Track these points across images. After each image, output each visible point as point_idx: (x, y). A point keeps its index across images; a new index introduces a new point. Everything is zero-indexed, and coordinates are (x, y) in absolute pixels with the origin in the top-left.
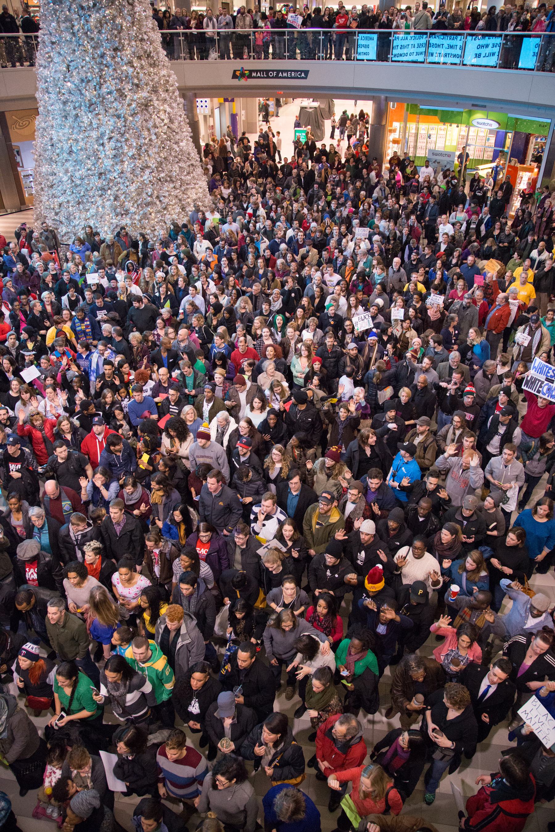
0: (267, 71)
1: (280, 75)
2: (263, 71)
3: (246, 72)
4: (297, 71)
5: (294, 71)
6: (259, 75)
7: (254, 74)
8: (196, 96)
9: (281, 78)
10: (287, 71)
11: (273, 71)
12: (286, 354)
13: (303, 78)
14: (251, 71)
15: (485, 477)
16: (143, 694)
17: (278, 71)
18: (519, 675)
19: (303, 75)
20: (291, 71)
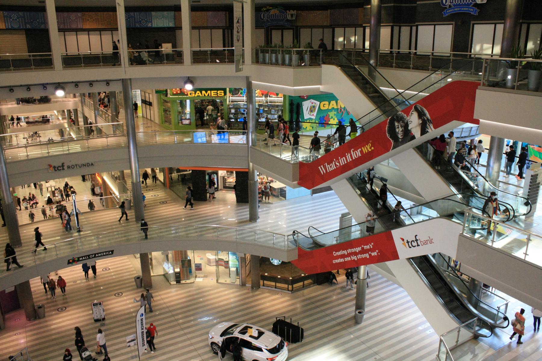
0: (89, 256)
1: (97, 255)
2: (86, 256)
3: (76, 259)
4: (107, 252)
5: (105, 252)
6: (84, 258)
7: (81, 259)
8: (272, 29)
9: (97, 257)
10: (101, 253)
11: (92, 255)
12: (291, 122)
13: (111, 254)
14: (79, 258)
15: (322, 40)
16: (506, 153)
17: (95, 254)
18: (379, 195)
19: (110, 253)
20: (103, 252)
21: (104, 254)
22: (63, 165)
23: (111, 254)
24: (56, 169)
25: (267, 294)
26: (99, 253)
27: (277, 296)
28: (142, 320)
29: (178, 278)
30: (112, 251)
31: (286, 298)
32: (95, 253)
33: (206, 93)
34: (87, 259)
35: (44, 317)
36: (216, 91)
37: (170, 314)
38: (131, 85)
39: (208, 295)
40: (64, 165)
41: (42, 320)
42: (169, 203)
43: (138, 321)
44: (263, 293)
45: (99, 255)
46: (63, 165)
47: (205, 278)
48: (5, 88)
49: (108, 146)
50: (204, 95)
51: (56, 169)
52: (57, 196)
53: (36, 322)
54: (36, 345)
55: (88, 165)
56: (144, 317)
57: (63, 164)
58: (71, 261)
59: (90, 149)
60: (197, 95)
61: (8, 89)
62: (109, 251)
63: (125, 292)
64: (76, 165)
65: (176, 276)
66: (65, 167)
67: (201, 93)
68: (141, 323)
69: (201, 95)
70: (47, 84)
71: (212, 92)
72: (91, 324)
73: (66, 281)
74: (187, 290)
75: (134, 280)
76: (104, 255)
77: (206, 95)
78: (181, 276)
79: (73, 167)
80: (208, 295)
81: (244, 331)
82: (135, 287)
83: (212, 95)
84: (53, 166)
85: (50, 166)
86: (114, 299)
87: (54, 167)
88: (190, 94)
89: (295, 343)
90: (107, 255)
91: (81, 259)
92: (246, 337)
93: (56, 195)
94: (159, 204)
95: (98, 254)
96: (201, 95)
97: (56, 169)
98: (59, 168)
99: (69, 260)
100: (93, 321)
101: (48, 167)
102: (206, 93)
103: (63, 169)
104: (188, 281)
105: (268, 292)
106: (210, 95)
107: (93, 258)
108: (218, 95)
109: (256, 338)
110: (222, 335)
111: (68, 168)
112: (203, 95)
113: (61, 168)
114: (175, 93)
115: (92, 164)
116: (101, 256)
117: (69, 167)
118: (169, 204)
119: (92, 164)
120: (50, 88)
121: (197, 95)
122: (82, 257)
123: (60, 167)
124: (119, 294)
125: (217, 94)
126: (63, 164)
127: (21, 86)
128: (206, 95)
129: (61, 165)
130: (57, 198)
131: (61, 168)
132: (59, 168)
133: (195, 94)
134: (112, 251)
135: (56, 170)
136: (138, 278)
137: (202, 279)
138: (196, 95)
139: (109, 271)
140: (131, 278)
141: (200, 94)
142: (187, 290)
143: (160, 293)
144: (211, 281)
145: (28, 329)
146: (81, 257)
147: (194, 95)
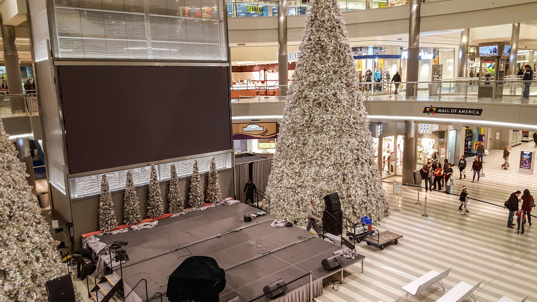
0: (450, 109)
1: (460, 111)
4: (473, 110)
5: (471, 110)
7: (440, 111)
11: (454, 109)
13: (477, 115)
14: (437, 109)
17: (458, 109)
19: (477, 112)
21: (470, 112)
30: (480, 111)
58: (428, 109)
62: (477, 110)
90: (473, 114)
91: (440, 111)
95: (462, 109)
99: (426, 108)
107: (454, 113)
122: (442, 109)
134: (480, 111)
146: (440, 108)
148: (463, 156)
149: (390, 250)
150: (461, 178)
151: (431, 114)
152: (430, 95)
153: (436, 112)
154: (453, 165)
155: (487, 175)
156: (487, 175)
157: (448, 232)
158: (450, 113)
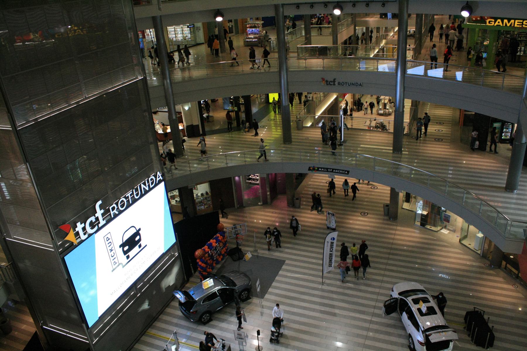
0: (327, 169)
1: (334, 171)
2: (325, 168)
4: (343, 170)
5: (342, 170)
6: (322, 170)
7: (320, 169)
10: (338, 170)
11: (330, 169)
13: (346, 174)
14: (318, 168)
17: (333, 169)
19: (346, 172)
20: (340, 170)
21: (341, 171)
22: (334, 81)
23: (346, 174)
24: (328, 83)
25: (501, 279)
26: (337, 170)
27: (510, 287)
28: (332, 243)
29: (424, 220)
30: (348, 172)
31: (520, 295)
32: (345, 170)
33: (509, 22)
34: (325, 171)
35: (299, 207)
36: (522, 21)
37: (389, 251)
38: (407, 7)
39: (439, 250)
40: (336, 80)
41: (297, 210)
42: (445, 142)
43: (328, 242)
44: (497, 276)
45: (337, 171)
46: (334, 81)
47: (452, 232)
48: (292, 5)
49: (306, 67)
50: (506, 24)
51: (328, 83)
52: (388, 109)
53: (292, 209)
54: (374, 231)
55: (357, 84)
56: (335, 241)
57: (335, 79)
58: (311, 168)
59: (307, 69)
60: (497, 23)
61: (323, 5)
62: (346, 171)
63: (371, 214)
64: (346, 83)
65: (421, 218)
66: (336, 83)
67: (503, 23)
68: (331, 245)
69: (502, 25)
70: (328, 2)
71: (517, 21)
72: (323, 229)
73: (336, 186)
74: (427, 236)
75: (382, 205)
76: (340, 173)
77: (508, 25)
78: (429, 220)
79: (343, 84)
80: (439, 250)
81: (416, 301)
82: (383, 213)
83: (516, 26)
84: (326, 79)
85: (323, 79)
86: (359, 216)
87: (327, 81)
88: (489, 22)
89: (477, 346)
90: (343, 173)
91: (320, 169)
92: (414, 308)
93: (387, 107)
94: (433, 140)
95: (335, 170)
96: (502, 25)
97: (328, 83)
98: (331, 83)
99: (310, 167)
100: (326, 227)
101: (321, 80)
102: (509, 22)
103: (334, 84)
104: (433, 228)
105: (504, 278)
106: (513, 25)
107: (330, 172)
108: (524, 26)
109: (422, 314)
110: (400, 294)
111: (338, 84)
112: (504, 25)
113: (333, 83)
114: (474, 19)
115: (360, 85)
116: (338, 173)
117: (339, 84)
118: (444, 144)
119: (360, 85)
120: (330, 6)
121: (497, 23)
122: (322, 168)
123: (332, 82)
124: (364, 214)
125: (523, 24)
126: (335, 79)
127: (306, 3)
128: (508, 25)
129: (332, 80)
130: (387, 111)
131: (333, 83)
132: (331, 83)
133: (495, 22)
134: (348, 172)
135: (327, 84)
136: (387, 206)
137: (448, 232)
138: (495, 25)
139: (376, 190)
140: (381, 203)
141: (501, 24)
142: (427, 236)
143: (399, 228)
144: (455, 238)
145: (283, 212)
146: (320, 168)
147: (493, 23)
148: (371, 96)
149: (214, 328)
150: (330, 195)
151: (314, 171)
152: (359, 343)
153: (318, 170)
154: (443, 313)
155: (197, 153)
156: (197, 153)
157: (294, 327)
158: (327, 171)
